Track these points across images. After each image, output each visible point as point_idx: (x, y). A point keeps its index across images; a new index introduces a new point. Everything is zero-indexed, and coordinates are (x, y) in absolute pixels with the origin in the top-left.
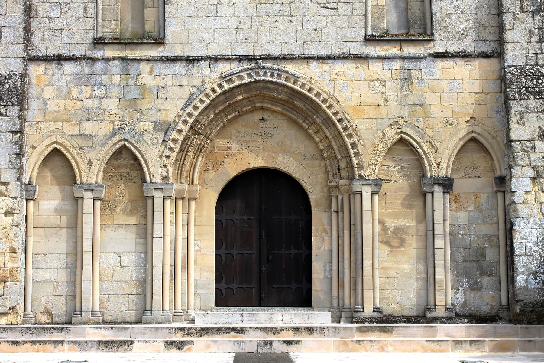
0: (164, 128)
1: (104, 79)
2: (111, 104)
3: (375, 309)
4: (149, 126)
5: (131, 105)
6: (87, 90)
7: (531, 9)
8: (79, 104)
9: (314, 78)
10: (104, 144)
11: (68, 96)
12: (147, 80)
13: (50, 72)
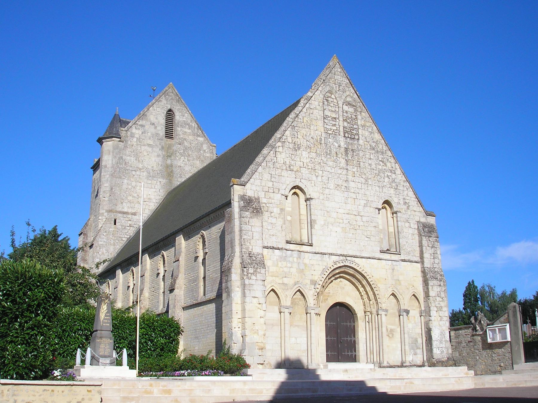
0: (314, 283)
1: (291, 259)
2: (294, 270)
3: (388, 363)
4: (309, 282)
5: (301, 271)
6: (284, 263)
7: (431, 246)
8: (282, 269)
9: (362, 265)
10: (292, 288)
11: (277, 266)
12: (306, 261)
13: (269, 254)
